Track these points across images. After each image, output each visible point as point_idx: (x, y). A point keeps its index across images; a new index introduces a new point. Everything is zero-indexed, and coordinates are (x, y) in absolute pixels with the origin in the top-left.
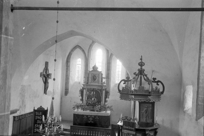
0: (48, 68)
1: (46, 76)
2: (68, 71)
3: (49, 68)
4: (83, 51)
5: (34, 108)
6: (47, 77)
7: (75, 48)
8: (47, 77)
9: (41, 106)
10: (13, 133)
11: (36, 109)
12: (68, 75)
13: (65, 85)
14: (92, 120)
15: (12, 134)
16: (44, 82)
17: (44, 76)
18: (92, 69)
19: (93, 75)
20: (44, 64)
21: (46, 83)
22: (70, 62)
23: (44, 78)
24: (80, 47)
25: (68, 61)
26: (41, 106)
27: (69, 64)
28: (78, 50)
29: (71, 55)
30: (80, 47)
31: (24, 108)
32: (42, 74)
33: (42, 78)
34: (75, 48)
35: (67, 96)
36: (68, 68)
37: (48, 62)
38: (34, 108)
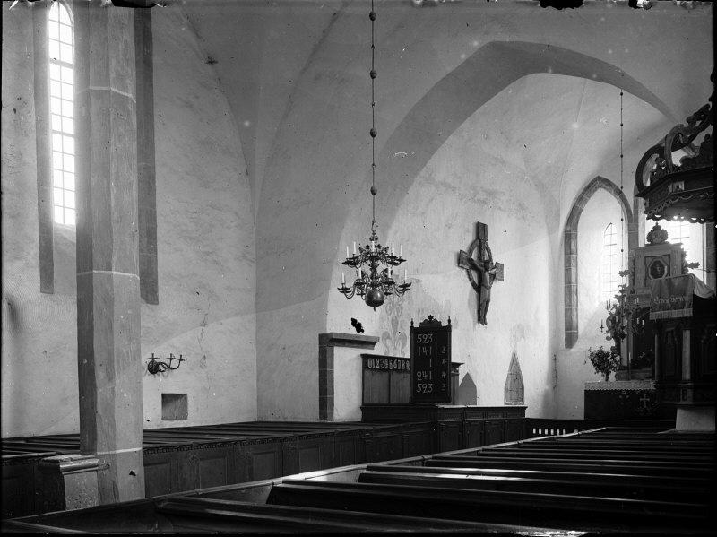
0: (488, 242)
1: (479, 267)
2: (573, 269)
3: (490, 242)
4: (619, 193)
5: (412, 323)
6: (483, 269)
7: (589, 189)
8: (483, 269)
9: (431, 317)
10: (367, 402)
11: (417, 325)
12: (573, 280)
13: (565, 314)
14: (647, 402)
15: (363, 404)
16: (473, 284)
17: (473, 266)
18: (647, 242)
19: (650, 259)
20: (472, 228)
21: (482, 287)
22: (576, 238)
23: (474, 274)
24: (607, 184)
25: (570, 237)
26: (431, 317)
27: (573, 244)
28: (601, 194)
29: (580, 213)
30: (607, 184)
31: (401, 344)
32: (464, 256)
33: (464, 272)
34: (589, 189)
35: (572, 350)
36: (570, 257)
37: (484, 226)
38: (412, 323)
